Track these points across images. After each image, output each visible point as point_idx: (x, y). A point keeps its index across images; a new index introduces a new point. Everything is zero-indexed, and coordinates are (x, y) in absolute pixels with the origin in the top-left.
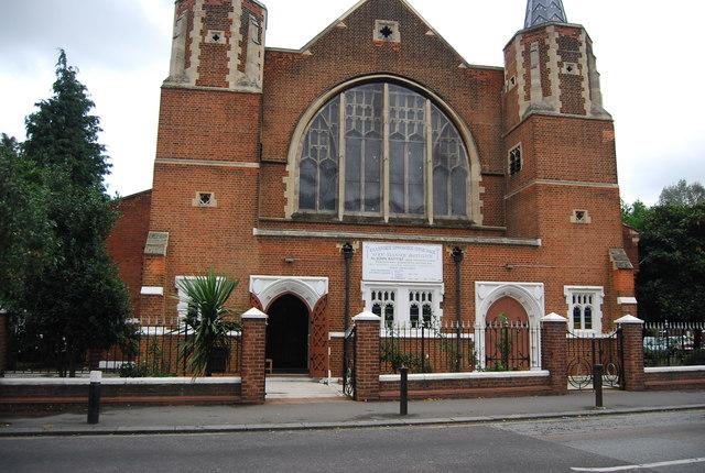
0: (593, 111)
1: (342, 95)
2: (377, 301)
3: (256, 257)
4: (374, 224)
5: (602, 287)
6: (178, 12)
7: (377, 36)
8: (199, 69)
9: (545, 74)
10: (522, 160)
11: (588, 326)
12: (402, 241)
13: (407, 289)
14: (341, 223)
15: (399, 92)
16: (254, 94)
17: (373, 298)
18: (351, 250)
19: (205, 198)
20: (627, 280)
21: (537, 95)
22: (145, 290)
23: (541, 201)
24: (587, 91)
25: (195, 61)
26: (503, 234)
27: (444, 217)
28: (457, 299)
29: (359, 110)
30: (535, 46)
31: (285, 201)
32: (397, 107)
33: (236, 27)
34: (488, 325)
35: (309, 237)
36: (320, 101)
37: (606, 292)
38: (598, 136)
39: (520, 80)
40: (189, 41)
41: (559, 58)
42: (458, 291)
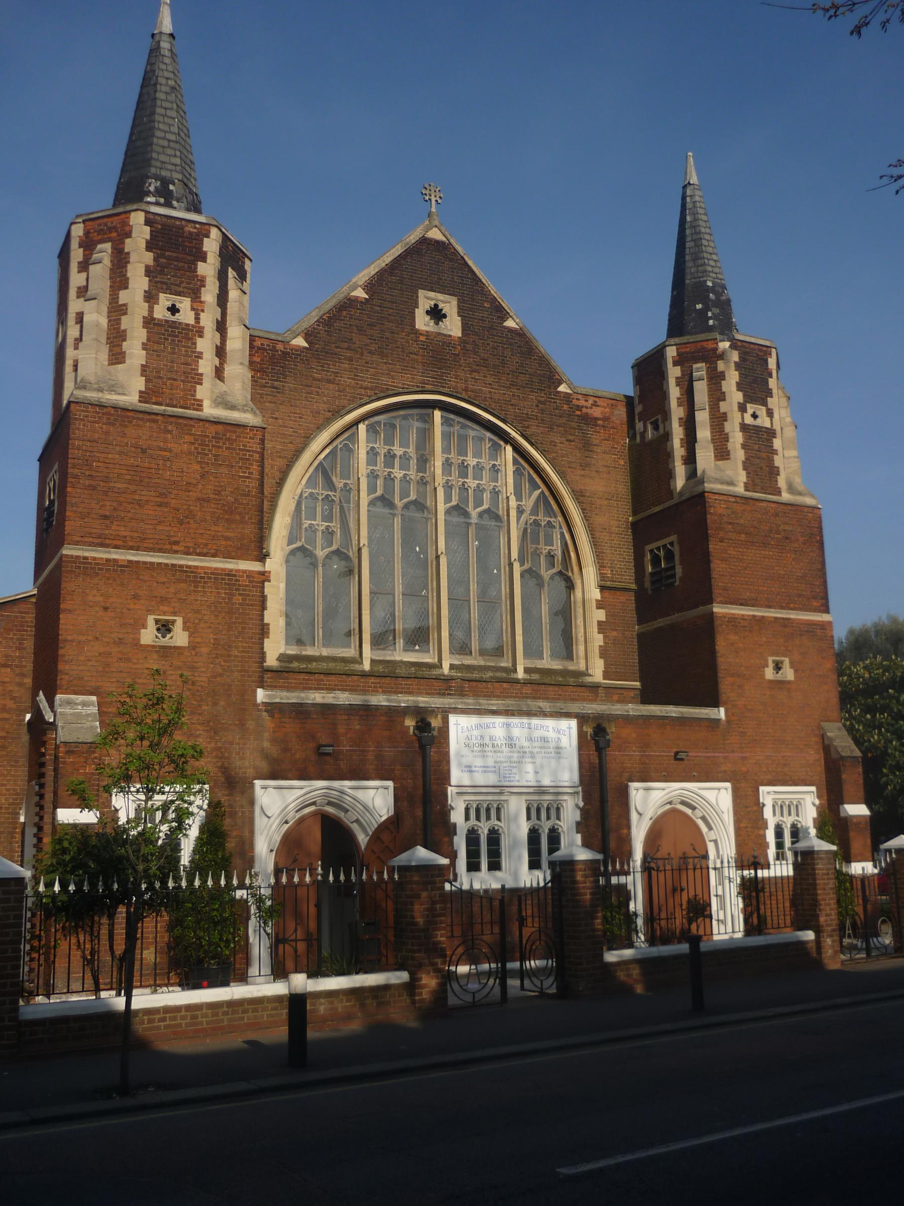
1: (362, 427)
5: (813, 789)
8: (144, 369)
9: (718, 420)
10: (679, 570)
11: (495, 866)
13: (524, 797)
20: (853, 778)
29: (390, 457)
31: (264, 631)
33: (209, 295)
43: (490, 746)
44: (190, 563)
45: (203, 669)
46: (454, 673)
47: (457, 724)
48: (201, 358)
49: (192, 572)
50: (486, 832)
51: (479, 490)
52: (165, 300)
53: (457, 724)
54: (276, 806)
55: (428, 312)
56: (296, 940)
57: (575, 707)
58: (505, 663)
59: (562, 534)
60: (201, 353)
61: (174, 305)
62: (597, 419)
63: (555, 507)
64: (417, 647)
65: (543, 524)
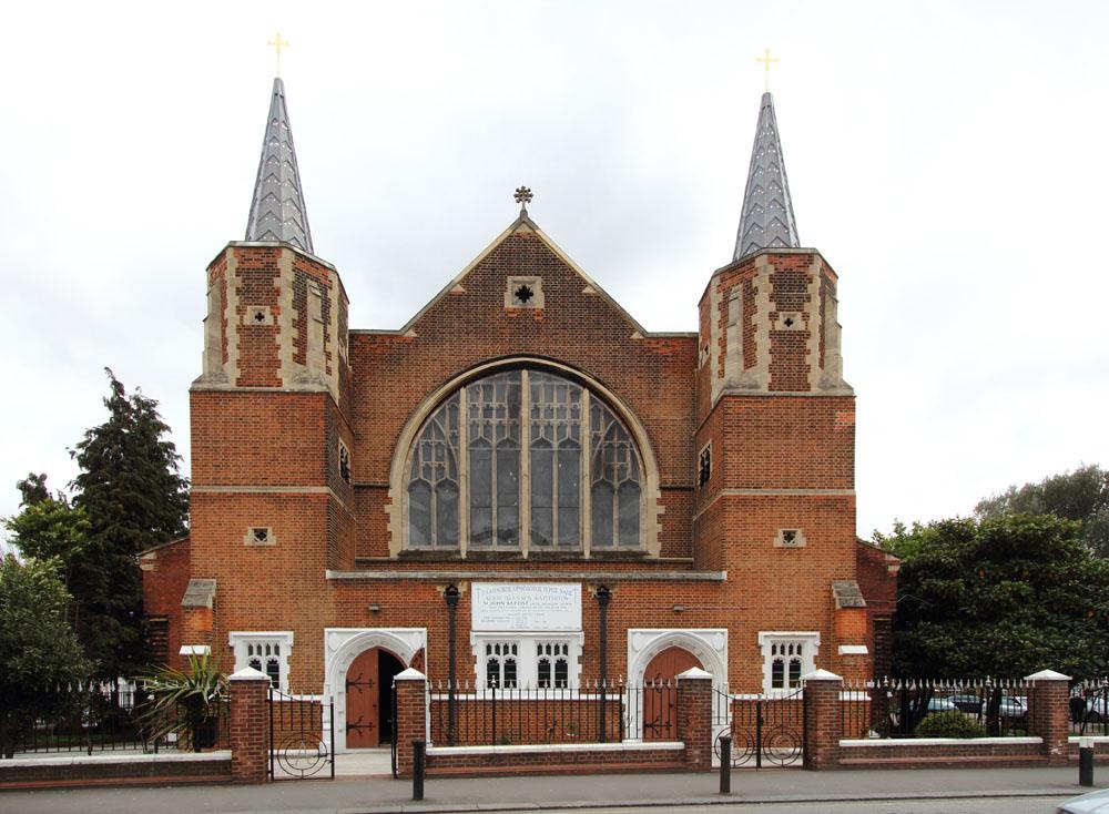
0: (824, 384)
1: (463, 390)
2: (778, 655)
3: (332, 605)
4: (478, 561)
5: (818, 634)
6: (211, 283)
7: (510, 302)
8: (239, 363)
12: (526, 580)
14: (526, 562)
15: (542, 381)
16: (318, 394)
17: (774, 652)
18: (456, 593)
19: (261, 534)
20: (855, 623)
21: (734, 367)
22: (185, 650)
23: (730, 519)
24: (816, 354)
25: (234, 352)
26: (690, 566)
27: (608, 548)
28: (603, 653)
29: (488, 411)
30: (738, 291)
32: (542, 404)
33: (286, 299)
34: (649, 683)
35: (401, 579)
36: (432, 401)
37: (823, 639)
38: (831, 423)
39: (715, 348)
40: (224, 324)
41: (772, 307)
42: (603, 641)
50: (789, 662)
51: (561, 427)
54: (341, 645)
55: (517, 294)
59: (632, 453)
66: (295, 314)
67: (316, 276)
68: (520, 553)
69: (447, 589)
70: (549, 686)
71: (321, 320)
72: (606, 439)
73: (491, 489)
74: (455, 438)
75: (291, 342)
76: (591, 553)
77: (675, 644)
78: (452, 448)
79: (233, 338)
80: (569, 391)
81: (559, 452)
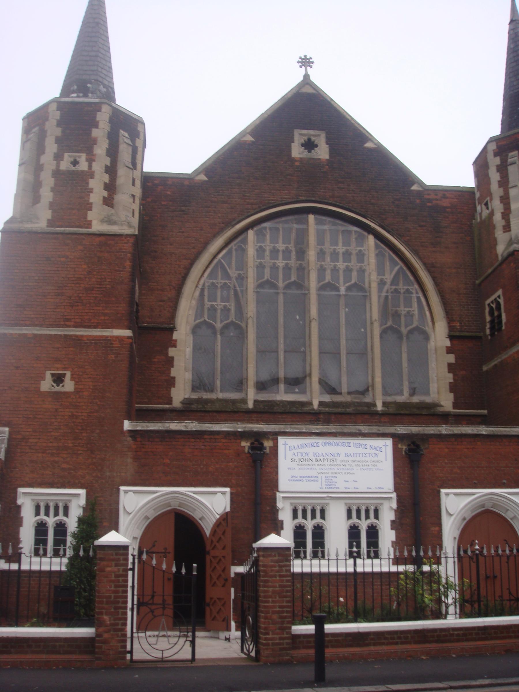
2: (300, 520)
15: (329, 225)
25: (47, 194)
29: (275, 252)
36: (219, 242)
43: (314, 460)
44: (78, 333)
45: (84, 407)
46: (323, 409)
47: (285, 444)
48: (92, 192)
49: (79, 340)
52: (67, 157)
53: (285, 444)
54: (137, 504)
55: (303, 145)
56: (510, 600)
57: (391, 430)
58: (368, 399)
59: (418, 298)
60: (92, 189)
61: (75, 160)
62: (445, 207)
63: (412, 278)
64: (297, 390)
65: (402, 291)
66: (108, 161)
67: (128, 129)
68: (310, 403)
69: (252, 444)
70: (305, 557)
71: (131, 167)
72: (392, 284)
73: (277, 333)
74: (242, 278)
75: (102, 186)
76: (384, 403)
77: (488, 506)
78: (238, 289)
79: (48, 181)
80: (354, 236)
81: (345, 295)
